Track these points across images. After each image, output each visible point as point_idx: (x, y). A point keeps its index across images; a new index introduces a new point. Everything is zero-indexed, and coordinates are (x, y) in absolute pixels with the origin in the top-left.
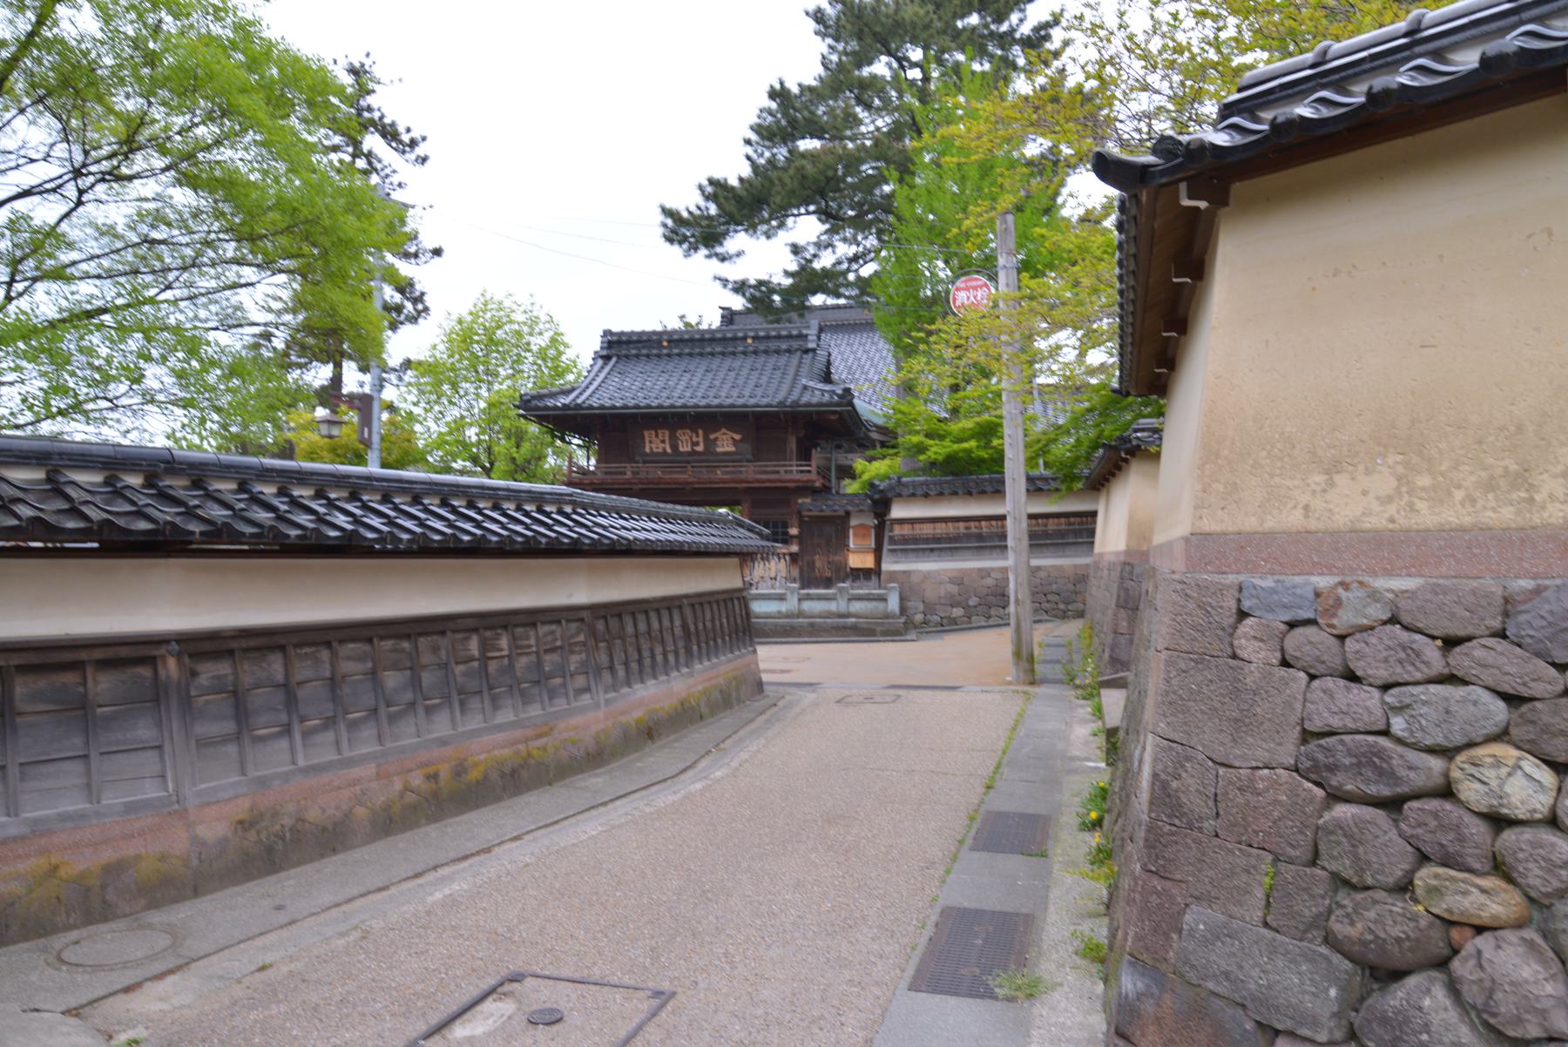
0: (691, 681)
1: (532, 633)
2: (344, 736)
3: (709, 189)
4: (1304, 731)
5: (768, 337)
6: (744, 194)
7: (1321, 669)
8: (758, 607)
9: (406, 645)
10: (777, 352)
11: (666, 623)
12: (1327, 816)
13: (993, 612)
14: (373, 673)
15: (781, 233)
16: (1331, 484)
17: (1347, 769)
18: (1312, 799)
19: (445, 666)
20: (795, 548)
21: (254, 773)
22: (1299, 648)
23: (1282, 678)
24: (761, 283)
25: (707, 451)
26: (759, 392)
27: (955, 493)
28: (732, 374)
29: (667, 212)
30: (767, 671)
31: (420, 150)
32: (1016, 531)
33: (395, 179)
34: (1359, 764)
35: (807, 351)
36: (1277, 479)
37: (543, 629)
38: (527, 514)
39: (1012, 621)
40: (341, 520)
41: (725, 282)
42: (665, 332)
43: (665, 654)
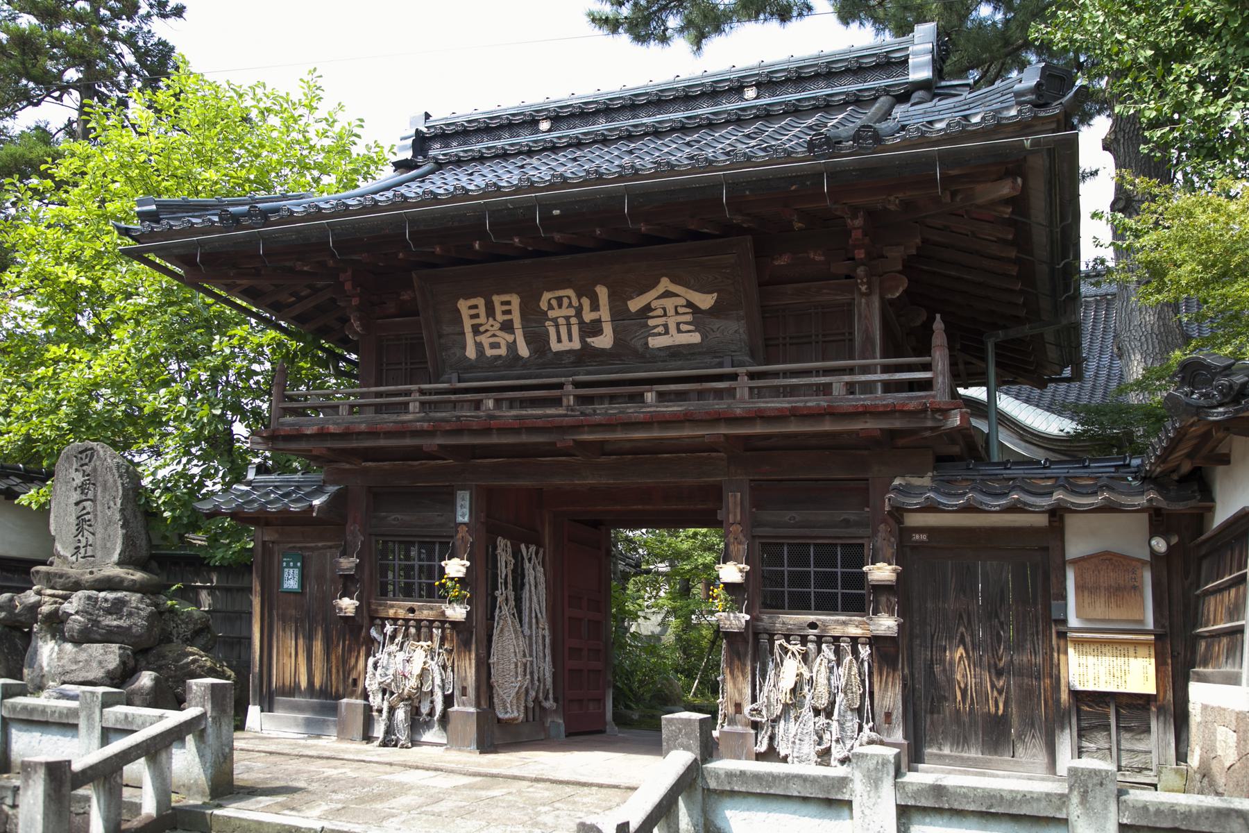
20: (886, 624)
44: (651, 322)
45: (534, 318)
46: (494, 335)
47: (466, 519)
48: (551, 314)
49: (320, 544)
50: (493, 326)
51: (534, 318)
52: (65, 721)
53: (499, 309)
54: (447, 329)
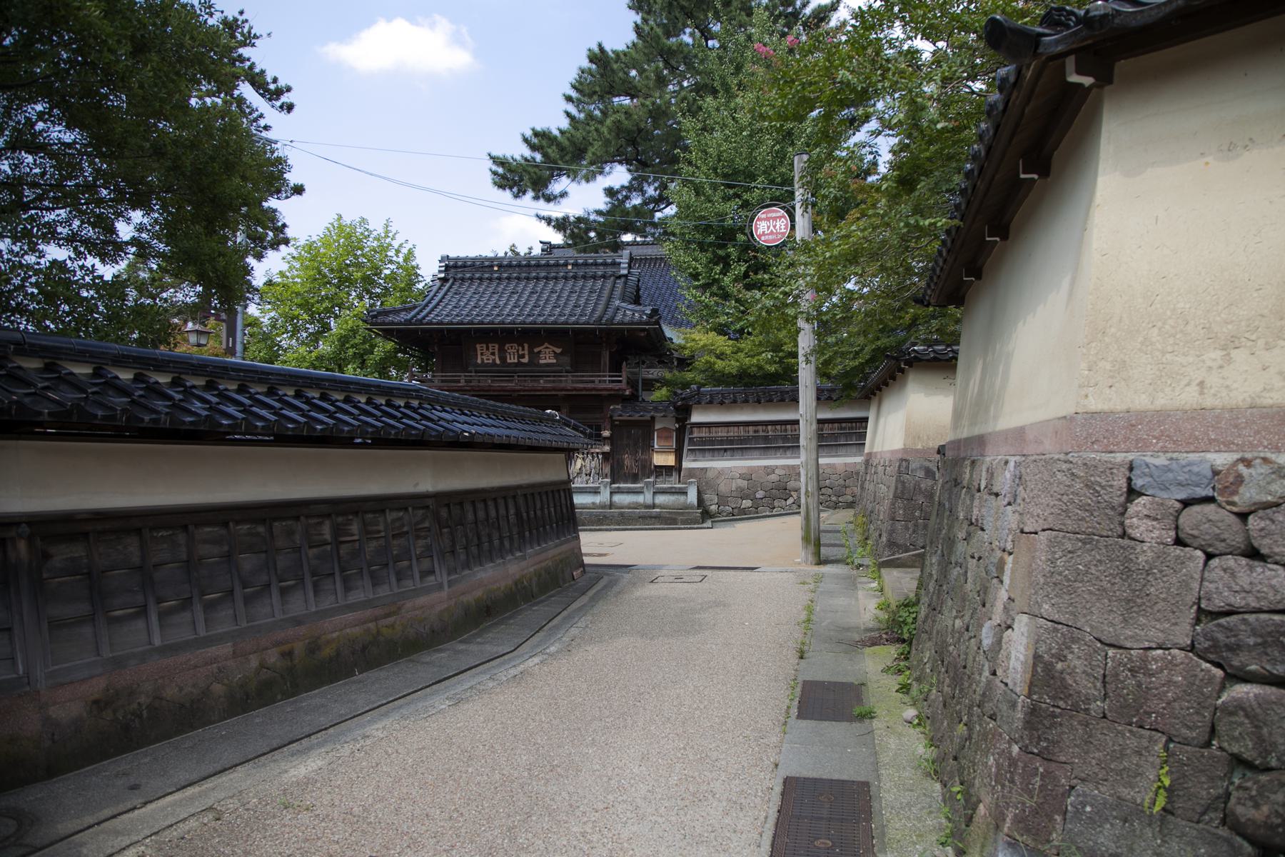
0: (524, 563)
1: (381, 519)
2: (200, 616)
3: (535, 140)
4: (1200, 609)
5: (586, 264)
6: (566, 143)
7: (1221, 547)
8: (578, 499)
9: (261, 529)
10: (594, 277)
11: (502, 511)
12: (1225, 697)
13: (776, 503)
14: (228, 557)
15: (599, 178)
16: (1228, 359)
17: (1250, 648)
18: (1211, 679)
19: (298, 550)
20: (607, 448)
21: (107, 653)
22: (1197, 527)
23: (1178, 557)
24: (579, 220)
25: (531, 363)
26: (578, 311)
27: (746, 401)
28: (555, 296)
29: (495, 160)
30: (587, 555)
31: (285, 98)
32: (806, 432)
33: (262, 122)
34: (1264, 644)
35: (620, 277)
36: (1168, 356)
37: (391, 516)
38: (377, 407)
39: (803, 510)
40: (197, 406)
41: (549, 221)
42: (496, 258)
43: (501, 539)
51: (502, 352)
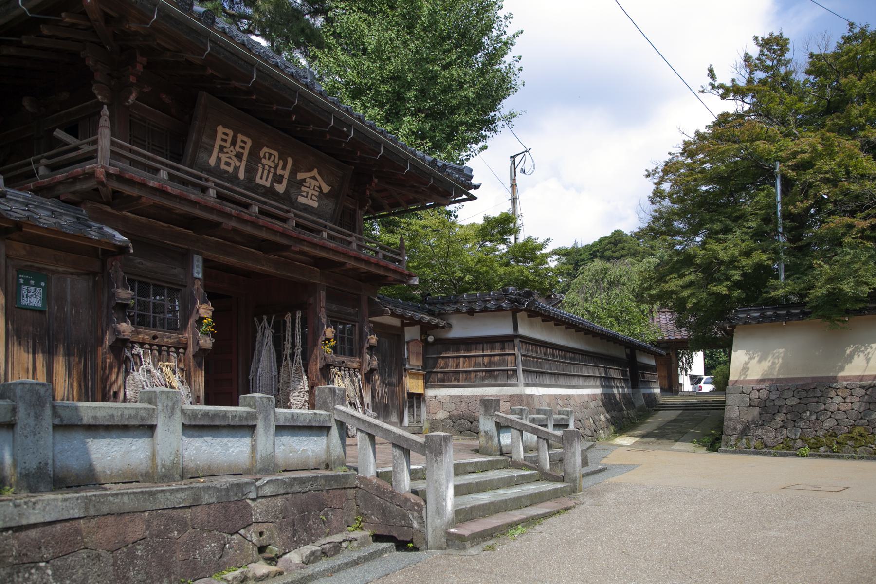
44: (303, 188)
45: (254, 157)
46: (230, 158)
47: (200, 276)
48: (264, 161)
49: (61, 269)
50: (232, 151)
51: (254, 157)
52: (245, 423)
53: (239, 143)
54: (205, 139)
